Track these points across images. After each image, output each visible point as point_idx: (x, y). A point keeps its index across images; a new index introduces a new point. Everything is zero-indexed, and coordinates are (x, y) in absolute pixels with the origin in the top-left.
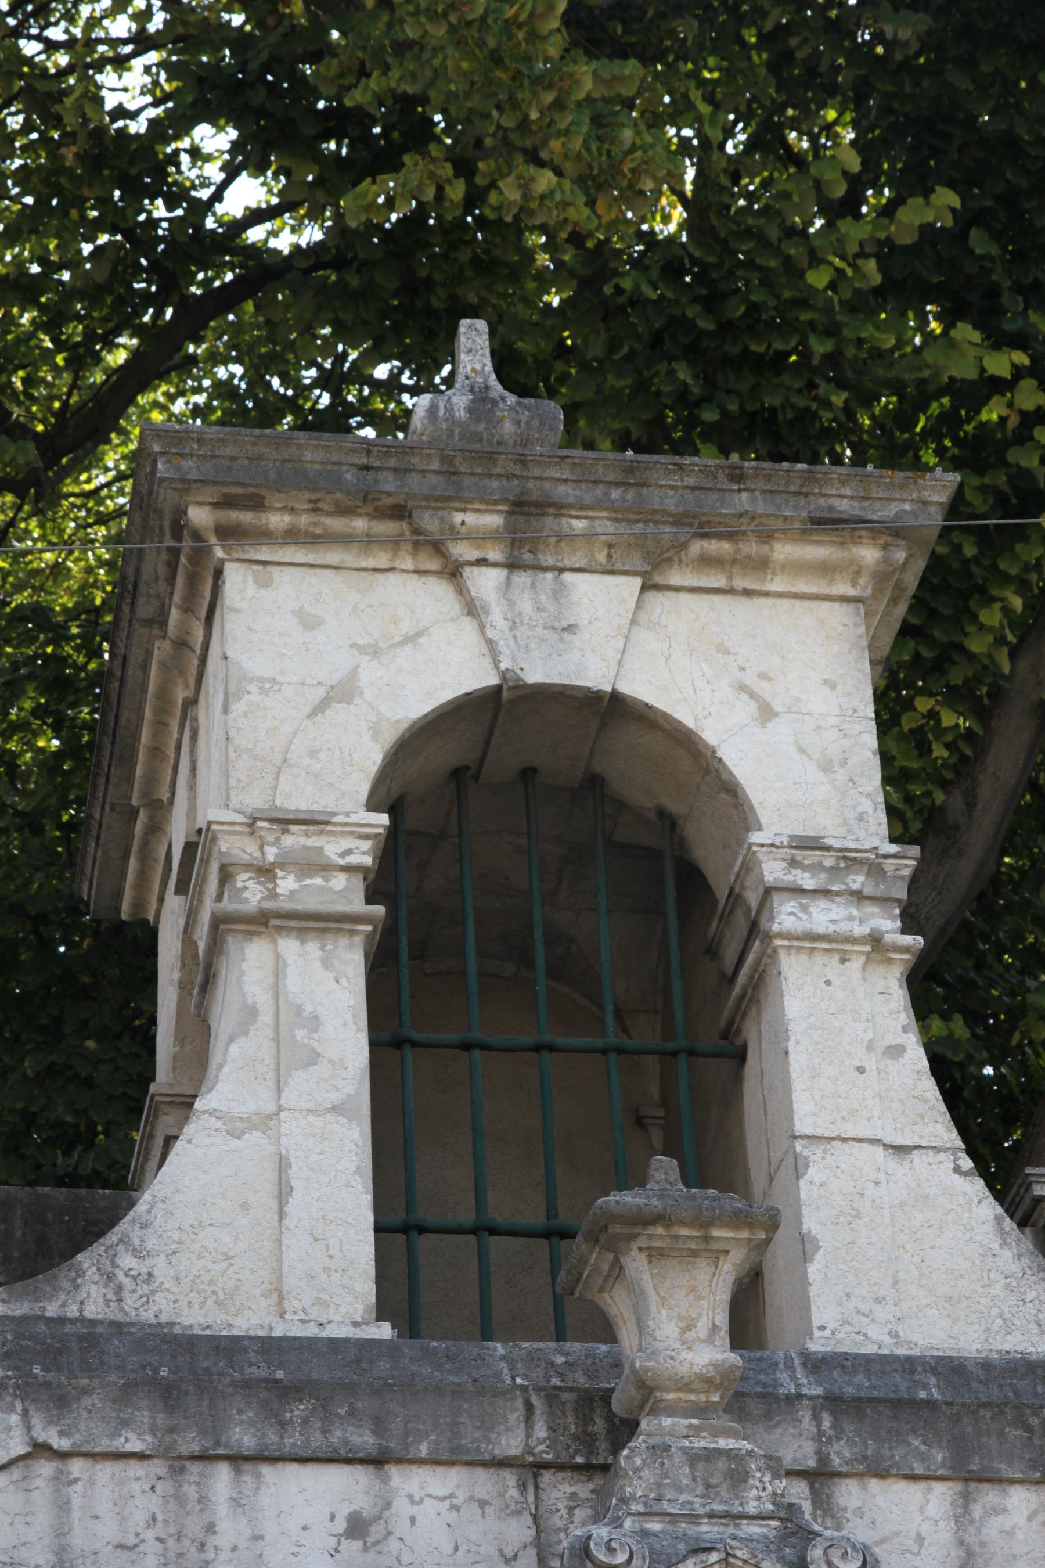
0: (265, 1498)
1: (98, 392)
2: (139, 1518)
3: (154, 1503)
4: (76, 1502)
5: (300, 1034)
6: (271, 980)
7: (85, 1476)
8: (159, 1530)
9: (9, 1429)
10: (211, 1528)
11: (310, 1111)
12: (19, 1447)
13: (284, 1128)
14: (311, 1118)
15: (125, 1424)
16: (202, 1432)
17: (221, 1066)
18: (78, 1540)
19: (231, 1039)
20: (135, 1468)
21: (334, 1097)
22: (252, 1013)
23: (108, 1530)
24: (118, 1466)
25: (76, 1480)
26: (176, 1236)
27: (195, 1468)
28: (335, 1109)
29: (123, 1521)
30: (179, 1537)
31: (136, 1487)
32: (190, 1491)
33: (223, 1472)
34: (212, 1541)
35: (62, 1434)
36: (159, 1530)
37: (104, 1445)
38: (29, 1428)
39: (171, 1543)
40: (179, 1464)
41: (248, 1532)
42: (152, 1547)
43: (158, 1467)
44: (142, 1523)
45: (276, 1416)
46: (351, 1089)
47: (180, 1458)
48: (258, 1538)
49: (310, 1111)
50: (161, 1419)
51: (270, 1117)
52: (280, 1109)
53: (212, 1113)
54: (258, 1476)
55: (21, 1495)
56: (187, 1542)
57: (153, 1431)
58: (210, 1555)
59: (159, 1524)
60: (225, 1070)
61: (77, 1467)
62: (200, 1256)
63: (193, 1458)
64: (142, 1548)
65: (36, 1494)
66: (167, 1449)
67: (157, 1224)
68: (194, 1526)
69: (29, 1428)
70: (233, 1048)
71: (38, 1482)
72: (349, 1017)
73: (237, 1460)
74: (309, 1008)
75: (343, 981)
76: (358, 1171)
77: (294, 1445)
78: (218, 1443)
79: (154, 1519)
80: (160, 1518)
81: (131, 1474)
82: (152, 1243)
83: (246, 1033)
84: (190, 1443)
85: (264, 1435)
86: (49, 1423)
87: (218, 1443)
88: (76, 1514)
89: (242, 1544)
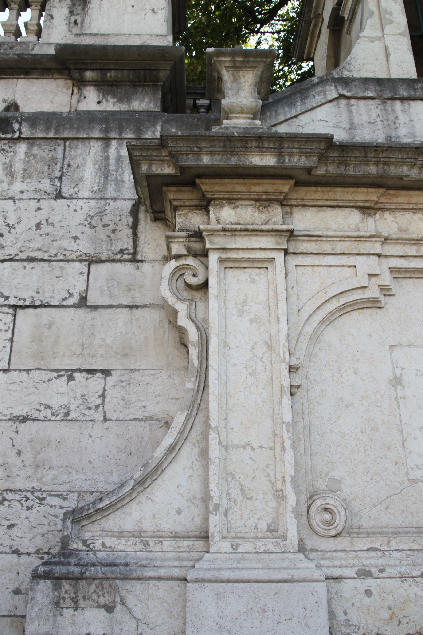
0: (412, 110)
1: (233, 137)
2: (374, 115)
3: (378, 111)
4: (354, 111)
5: (387, 16)
6: (376, 4)
7: (356, 104)
8: (381, 118)
9: (331, 90)
10: (397, 118)
11: (393, 35)
12: (335, 95)
13: (386, 39)
14: (393, 36)
15: (367, 89)
16: (391, 91)
17: (365, 26)
18: (356, 121)
19: (367, 19)
20: (370, 102)
21: (398, 31)
22: (372, 13)
23: (365, 118)
24: (366, 101)
25: (353, 105)
26: (359, 66)
27: (389, 102)
28: (399, 34)
29: (369, 116)
30: (387, 120)
31: (372, 107)
32: (389, 108)
33: (398, 104)
34: (397, 122)
35: (348, 92)
36: (381, 118)
37: (361, 95)
38: (337, 90)
39: (385, 122)
40: (384, 100)
41: (408, 119)
42: (379, 123)
43: (377, 102)
44: (375, 117)
45: (413, 87)
46: (403, 29)
47: (384, 99)
48: (412, 121)
49: (393, 35)
50: (377, 88)
51: (381, 37)
52: (384, 34)
53: (364, 37)
54: (409, 104)
55: (337, 109)
56: (390, 122)
57: (375, 91)
58: (398, 125)
59: (381, 117)
60: (367, 26)
61: (353, 101)
62: (366, 72)
63: (389, 99)
64: (376, 123)
65: (341, 109)
66: (380, 97)
67: (353, 63)
68: (392, 117)
69: (337, 90)
70: (368, 21)
71: (342, 105)
72: (400, 12)
73: (402, 99)
74: (388, 10)
75: (397, 3)
76: (408, 49)
77: (419, 95)
78: (396, 94)
79: (379, 115)
80: (381, 115)
81: (370, 103)
82: (352, 68)
83: (371, 18)
84: (387, 94)
85: (410, 92)
86: (343, 89)
87: (396, 94)
88: (355, 114)
89: (407, 122)
